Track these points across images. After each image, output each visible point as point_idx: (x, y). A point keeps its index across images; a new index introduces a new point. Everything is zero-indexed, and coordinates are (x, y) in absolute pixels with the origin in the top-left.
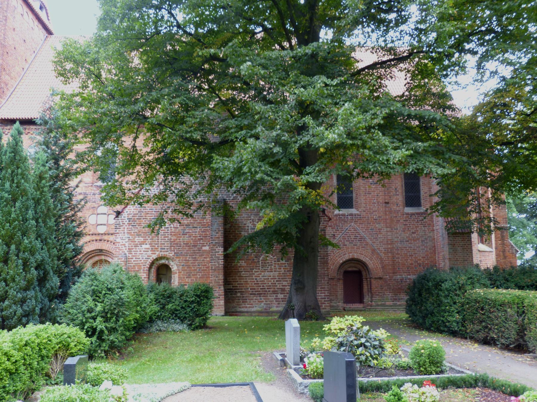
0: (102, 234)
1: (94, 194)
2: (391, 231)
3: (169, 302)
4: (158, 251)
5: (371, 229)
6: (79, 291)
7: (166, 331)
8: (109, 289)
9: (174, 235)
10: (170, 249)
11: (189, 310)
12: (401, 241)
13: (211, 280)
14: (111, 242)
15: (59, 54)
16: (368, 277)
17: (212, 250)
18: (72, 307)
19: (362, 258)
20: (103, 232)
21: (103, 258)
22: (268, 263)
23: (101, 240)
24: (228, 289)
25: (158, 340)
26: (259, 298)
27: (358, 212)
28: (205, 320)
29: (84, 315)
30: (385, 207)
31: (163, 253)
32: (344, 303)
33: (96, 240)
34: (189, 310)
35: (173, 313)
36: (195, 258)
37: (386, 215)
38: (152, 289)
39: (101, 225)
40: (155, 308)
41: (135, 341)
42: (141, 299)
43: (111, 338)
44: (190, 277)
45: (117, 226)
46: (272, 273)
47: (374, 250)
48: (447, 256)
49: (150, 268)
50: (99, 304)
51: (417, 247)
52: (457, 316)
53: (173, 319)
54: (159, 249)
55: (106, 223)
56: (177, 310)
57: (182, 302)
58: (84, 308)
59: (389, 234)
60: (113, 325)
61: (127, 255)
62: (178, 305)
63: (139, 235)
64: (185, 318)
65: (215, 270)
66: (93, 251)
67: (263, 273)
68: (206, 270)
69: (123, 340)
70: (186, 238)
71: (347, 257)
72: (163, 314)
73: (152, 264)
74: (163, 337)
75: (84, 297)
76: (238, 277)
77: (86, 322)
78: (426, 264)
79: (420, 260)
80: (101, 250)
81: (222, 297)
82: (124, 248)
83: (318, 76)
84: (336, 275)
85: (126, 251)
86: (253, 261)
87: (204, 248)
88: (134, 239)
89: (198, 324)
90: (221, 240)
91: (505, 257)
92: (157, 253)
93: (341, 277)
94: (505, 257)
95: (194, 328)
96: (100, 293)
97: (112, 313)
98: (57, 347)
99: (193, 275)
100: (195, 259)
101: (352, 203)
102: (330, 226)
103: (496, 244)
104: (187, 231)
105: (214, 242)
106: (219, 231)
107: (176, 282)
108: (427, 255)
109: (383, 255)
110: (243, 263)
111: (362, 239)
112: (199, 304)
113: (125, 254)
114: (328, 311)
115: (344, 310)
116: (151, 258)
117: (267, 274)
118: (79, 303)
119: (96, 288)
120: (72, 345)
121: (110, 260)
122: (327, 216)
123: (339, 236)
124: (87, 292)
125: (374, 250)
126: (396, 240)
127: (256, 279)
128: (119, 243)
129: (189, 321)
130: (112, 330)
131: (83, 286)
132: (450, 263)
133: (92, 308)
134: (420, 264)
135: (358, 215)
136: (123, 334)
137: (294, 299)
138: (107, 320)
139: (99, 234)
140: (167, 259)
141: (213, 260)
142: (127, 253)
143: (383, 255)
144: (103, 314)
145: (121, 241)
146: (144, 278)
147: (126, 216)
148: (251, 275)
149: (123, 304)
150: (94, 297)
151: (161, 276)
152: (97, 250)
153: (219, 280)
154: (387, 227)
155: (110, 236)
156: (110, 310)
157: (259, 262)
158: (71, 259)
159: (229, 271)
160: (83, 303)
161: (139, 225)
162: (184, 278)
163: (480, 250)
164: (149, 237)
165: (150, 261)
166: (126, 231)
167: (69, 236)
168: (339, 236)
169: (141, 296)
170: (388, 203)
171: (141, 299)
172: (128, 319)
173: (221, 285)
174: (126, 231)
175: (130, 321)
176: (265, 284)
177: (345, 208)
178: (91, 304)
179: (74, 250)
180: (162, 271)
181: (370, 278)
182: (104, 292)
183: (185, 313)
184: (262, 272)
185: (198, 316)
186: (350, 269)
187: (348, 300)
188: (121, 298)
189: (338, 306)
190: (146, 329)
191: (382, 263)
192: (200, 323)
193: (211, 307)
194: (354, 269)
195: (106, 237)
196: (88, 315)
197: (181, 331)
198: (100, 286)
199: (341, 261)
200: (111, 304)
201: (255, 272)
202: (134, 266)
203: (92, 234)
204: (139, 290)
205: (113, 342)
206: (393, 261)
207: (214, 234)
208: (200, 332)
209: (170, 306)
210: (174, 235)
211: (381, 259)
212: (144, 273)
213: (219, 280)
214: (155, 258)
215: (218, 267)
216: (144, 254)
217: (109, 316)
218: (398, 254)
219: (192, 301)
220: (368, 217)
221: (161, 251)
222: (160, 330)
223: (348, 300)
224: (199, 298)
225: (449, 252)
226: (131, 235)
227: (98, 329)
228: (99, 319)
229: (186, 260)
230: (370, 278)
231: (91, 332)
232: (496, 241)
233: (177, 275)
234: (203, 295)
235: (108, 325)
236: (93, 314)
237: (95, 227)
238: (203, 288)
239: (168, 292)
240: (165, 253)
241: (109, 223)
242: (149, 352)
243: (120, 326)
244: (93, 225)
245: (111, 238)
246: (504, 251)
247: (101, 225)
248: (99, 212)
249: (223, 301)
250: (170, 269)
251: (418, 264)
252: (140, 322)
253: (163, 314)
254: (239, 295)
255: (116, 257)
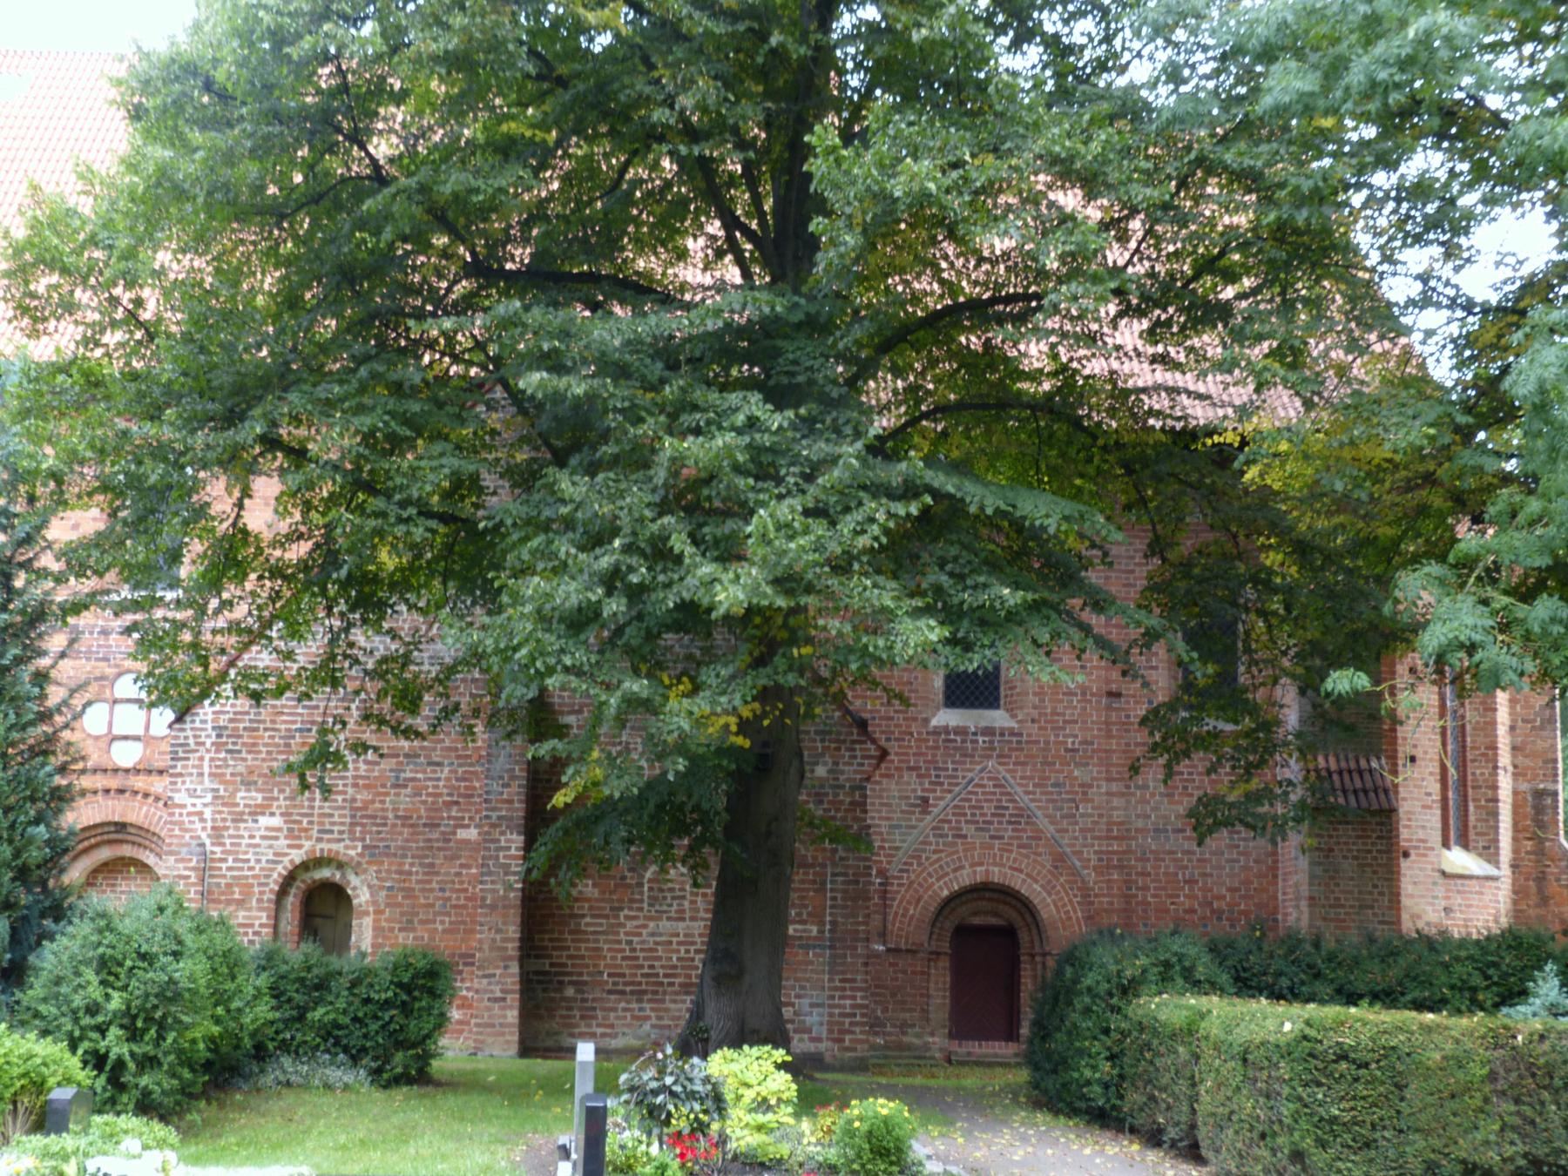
0: (127, 771)
1: (105, 632)
2: (1123, 795)
3: (317, 1003)
4: (309, 838)
5: (1055, 785)
6: (65, 958)
7: (305, 1087)
8: (143, 956)
9: (366, 786)
10: (352, 832)
11: (374, 1027)
12: (1157, 830)
13: (480, 941)
14: (157, 799)
15: (18, 252)
16: (1037, 949)
17: (487, 839)
18: (45, 1000)
19: (1018, 882)
20: (129, 764)
21: (127, 851)
22: (671, 890)
23: (121, 791)
24: (537, 973)
25: (276, 1105)
26: (635, 1005)
27: (1013, 724)
28: (426, 1057)
29: (76, 1020)
30: (1109, 708)
31: (325, 846)
32: (951, 1036)
33: (107, 791)
34: (374, 1027)
35: (329, 1034)
36: (432, 865)
37: (1109, 736)
38: (269, 960)
39: (126, 738)
40: (264, 1011)
41: (209, 1103)
42: (230, 986)
43: (144, 1081)
44: (414, 930)
45: (179, 752)
46: (681, 925)
47: (1060, 859)
48: (1305, 890)
49: (282, 892)
50: (115, 994)
51: (1213, 853)
52: (1106, 1066)
53: (327, 1051)
54: (315, 834)
55: (141, 732)
56: (340, 1027)
57: (357, 1002)
58: (78, 1001)
59: (1116, 802)
60: (148, 1049)
61: (209, 848)
62: (345, 1012)
63: (248, 784)
64: (364, 1050)
65: (493, 907)
66: (95, 826)
67: (652, 924)
68: (465, 907)
69: (172, 1092)
70: (405, 799)
71: (965, 878)
72: (299, 1035)
73: (289, 880)
74: (290, 1097)
75: (78, 974)
76: (571, 932)
77: (81, 1039)
78: (1242, 912)
79: (1221, 897)
80: (121, 827)
81: (514, 999)
82: (198, 825)
83: (741, 394)
84: (925, 938)
85: (204, 835)
86: (622, 883)
87: (462, 834)
88: (233, 795)
89: (399, 1070)
90: (519, 808)
91: (1544, 900)
92: (307, 844)
93: (946, 947)
94: (1544, 900)
95: (385, 1079)
96: (121, 965)
97: (149, 1020)
98: (18, 1084)
99: (422, 922)
100: (431, 870)
101: (997, 688)
102: (910, 769)
103: (1516, 851)
104: (409, 775)
105: (494, 815)
106: (513, 778)
107: (364, 935)
108: (1247, 882)
109: (1091, 876)
110: (588, 888)
111: (1021, 817)
112: (406, 1009)
113: (203, 845)
114: (862, 1059)
115: (949, 1061)
116: (286, 860)
117: (665, 925)
118: (64, 989)
119: (109, 951)
120: (52, 1081)
121: (150, 859)
122: (874, 741)
123: (942, 804)
124: (87, 962)
125: (1060, 859)
126: (1140, 824)
127: (629, 943)
128: (183, 806)
129: (375, 1058)
130: (147, 1063)
131: (75, 946)
132: (1311, 913)
133: (96, 1004)
134: (1218, 914)
135: (1012, 734)
136: (174, 1076)
137: (710, 1009)
138: (134, 1035)
139: (116, 771)
140: (340, 866)
141: (490, 873)
142: (208, 842)
143: (1091, 876)
144: (125, 1021)
145: (189, 801)
146: (252, 924)
147: (210, 717)
148: (613, 930)
149: (177, 997)
150: (104, 975)
151: (318, 921)
152: (109, 824)
153: (505, 940)
154: (1109, 780)
155: (155, 778)
156: (142, 1009)
157: (641, 885)
158: (39, 867)
159: (541, 917)
160: (75, 991)
161: (252, 748)
162: (392, 930)
163: (1448, 870)
164: (282, 791)
165: (281, 870)
166: (206, 770)
167: (33, 800)
168: (942, 804)
169: (233, 978)
170: (1118, 695)
171: (230, 986)
172: (190, 1035)
173: (510, 958)
174: (206, 770)
175: (194, 1041)
176: (659, 958)
177: (972, 706)
178: (95, 992)
179: (48, 842)
180: (318, 902)
181: (1044, 955)
182: (129, 963)
183: (365, 1036)
184: (651, 918)
185: (401, 1045)
186: (976, 921)
187: (966, 1024)
188: (171, 981)
189: (927, 1047)
190: (247, 1077)
191: (1087, 900)
192: (406, 1067)
193: (441, 1021)
194: (993, 921)
195: (139, 782)
196: (87, 1021)
197: (346, 1087)
198: (120, 946)
199: (946, 893)
200: (147, 995)
201: (627, 918)
202: (229, 885)
203: (95, 771)
204: (228, 963)
205: (146, 1093)
206: (1128, 898)
207: (495, 787)
208: (400, 1094)
209: (317, 1014)
210: (366, 786)
211: (1085, 891)
212: (260, 909)
213: (505, 940)
214: (298, 861)
215: (505, 897)
216: (266, 845)
217: (139, 1024)
218: (1145, 874)
219: (387, 1001)
220: (1047, 743)
221: (319, 840)
222: (288, 1084)
223: (966, 1024)
224: (409, 993)
225: (1312, 877)
226: (225, 782)
227: (112, 1056)
228: (114, 1032)
229: (400, 872)
230: (1044, 955)
231: (97, 1061)
232: (1515, 839)
233: (368, 922)
234: (422, 986)
235: (136, 1049)
236: (100, 1019)
237: (103, 744)
238: (420, 964)
239: (315, 971)
240: (334, 846)
241: (152, 732)
242: (242, 1128)
243: (166, 1054)
244: (97, 738)
245: (158, 785)
246: (1541, 879)
247: (126, 738)
248: (118, 695)
249: (516, 1013)
250: (348, 899)
251: (1213, 912)
252: (224, 1050)
253: (299, 1035)
254: (570, 992)
255: (171, 853)
